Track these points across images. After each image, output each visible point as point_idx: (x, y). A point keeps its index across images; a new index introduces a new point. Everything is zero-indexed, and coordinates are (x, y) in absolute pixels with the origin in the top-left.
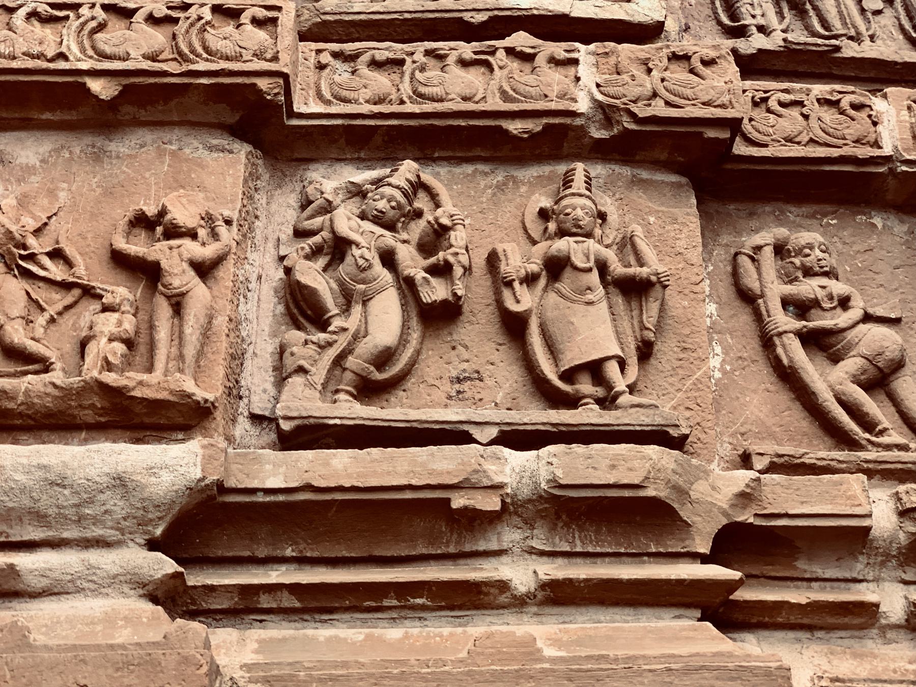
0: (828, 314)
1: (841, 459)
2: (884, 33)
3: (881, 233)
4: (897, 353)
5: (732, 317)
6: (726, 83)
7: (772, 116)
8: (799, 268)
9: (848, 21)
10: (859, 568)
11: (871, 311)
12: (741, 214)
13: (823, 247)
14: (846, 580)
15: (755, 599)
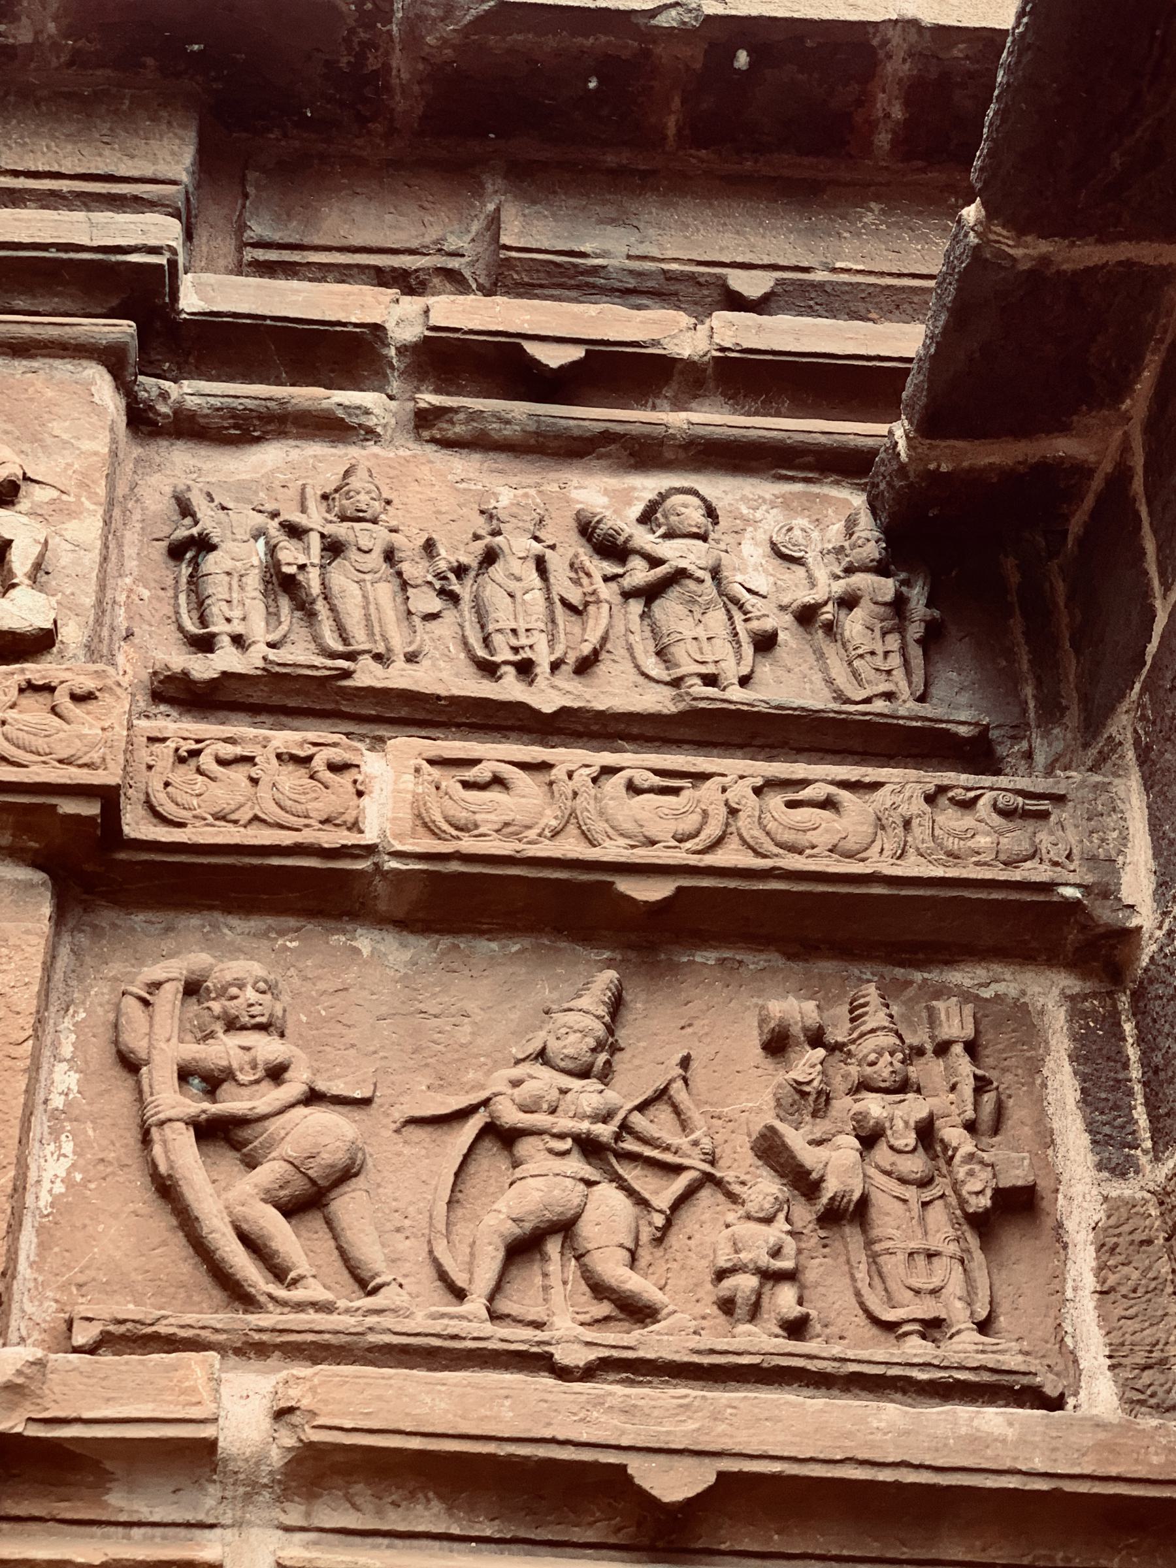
0: (245, 1092)
1: (219, 1326)
2: (436, 648)
3: (366, 963)
4: (340, 1155)
5: (101, 1094)
6: (103, 729)
7: (200, 778)
8: (218, 1018)
9: (377, 630)
10: (207, 1504)
11: (321, 1086)
12: (152, 929)
13: (262, 985)
14: (188, 1525)
15: (17, 1556)
